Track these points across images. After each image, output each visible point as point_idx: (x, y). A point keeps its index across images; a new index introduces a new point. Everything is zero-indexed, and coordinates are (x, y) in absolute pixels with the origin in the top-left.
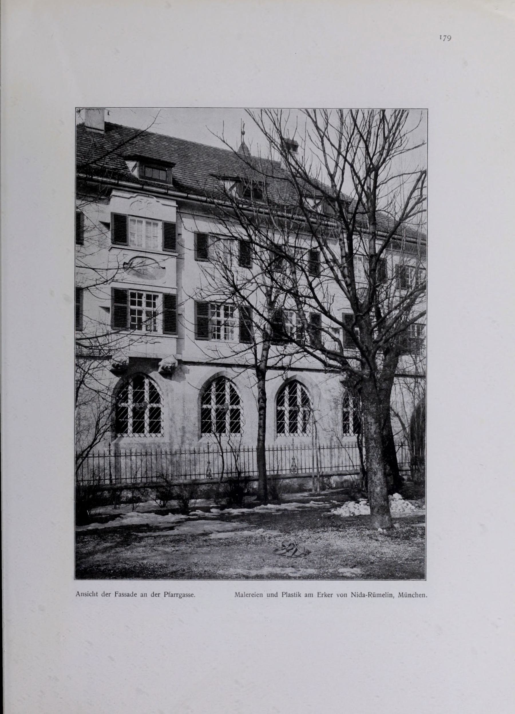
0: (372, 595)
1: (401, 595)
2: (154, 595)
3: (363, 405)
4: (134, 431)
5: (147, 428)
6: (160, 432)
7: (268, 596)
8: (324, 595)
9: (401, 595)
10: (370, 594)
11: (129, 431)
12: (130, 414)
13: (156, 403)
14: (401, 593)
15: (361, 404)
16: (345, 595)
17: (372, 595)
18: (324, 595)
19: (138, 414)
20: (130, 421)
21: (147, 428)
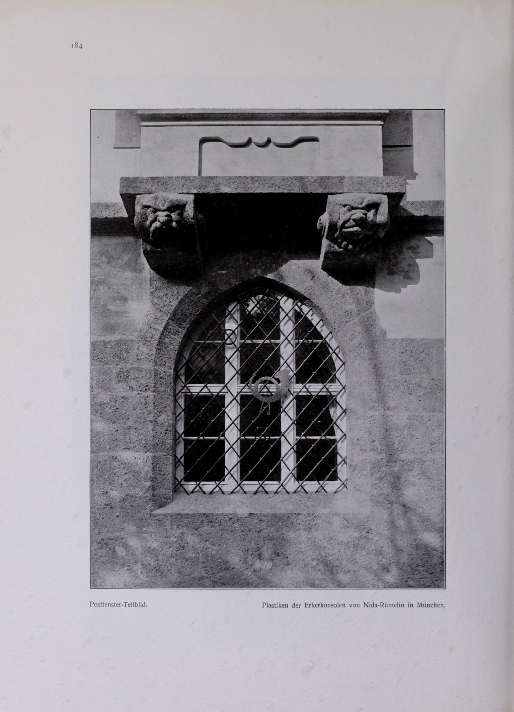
0: (384, 605)
1: (420, 605)
2: (295, 606)
3: (222, 275)
4: (301, 474)
5: (289, 462)
6: (334, 477)
7: (286, 606)
8: (311, 606)
9: (420, 605)
10: (382, 604)
11: (284, 473)
12: (233, 412)
13: (314, 381)
14: (420, 604)
15: (223, 272)
16: (358, 605)
17: (384, 605)
18: (311, 606)
19: (260, 416)
20: (232, 435)
21: (289, 462)
